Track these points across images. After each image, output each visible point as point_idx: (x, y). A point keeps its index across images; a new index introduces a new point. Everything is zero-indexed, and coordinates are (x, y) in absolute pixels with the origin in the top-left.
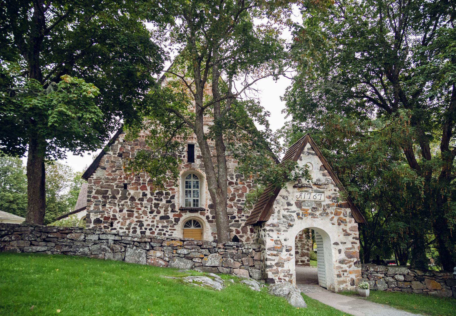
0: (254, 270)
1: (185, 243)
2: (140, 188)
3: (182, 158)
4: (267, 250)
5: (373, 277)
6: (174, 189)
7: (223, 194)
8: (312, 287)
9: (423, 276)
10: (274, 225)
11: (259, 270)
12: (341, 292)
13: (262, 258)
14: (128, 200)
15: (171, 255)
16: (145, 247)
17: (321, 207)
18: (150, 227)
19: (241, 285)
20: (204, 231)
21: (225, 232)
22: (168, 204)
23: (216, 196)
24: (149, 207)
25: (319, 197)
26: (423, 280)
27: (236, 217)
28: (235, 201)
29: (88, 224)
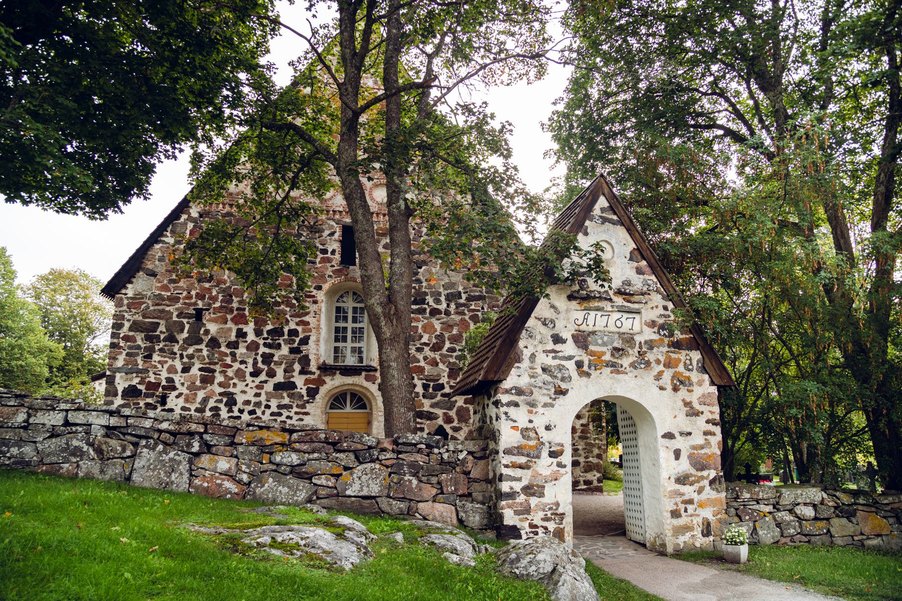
0: (469, 505)
1: (295, 436)
2: (232, 320)
3: (329, 255)
4: (501, 454)
5: (748, 514)
6: (308, 323)
7: (399, 318)
8: (610, 544)
9: (852, 504)
10: (520, 392)
11: (483, 503)
12: (680, 555)
13: (491, 475)
15: (256, 466)
16: (189, 445)
17: (633, 348)
18: (251, 408)
19: (420, 551)
20: (374, 416)
21: (402, 410)
22: (293, 356)
23: (383, 324)
25: (629, 324)
26: (854, 515)
27: (446, 385)
28: (444, 351)
29: (110, 398)
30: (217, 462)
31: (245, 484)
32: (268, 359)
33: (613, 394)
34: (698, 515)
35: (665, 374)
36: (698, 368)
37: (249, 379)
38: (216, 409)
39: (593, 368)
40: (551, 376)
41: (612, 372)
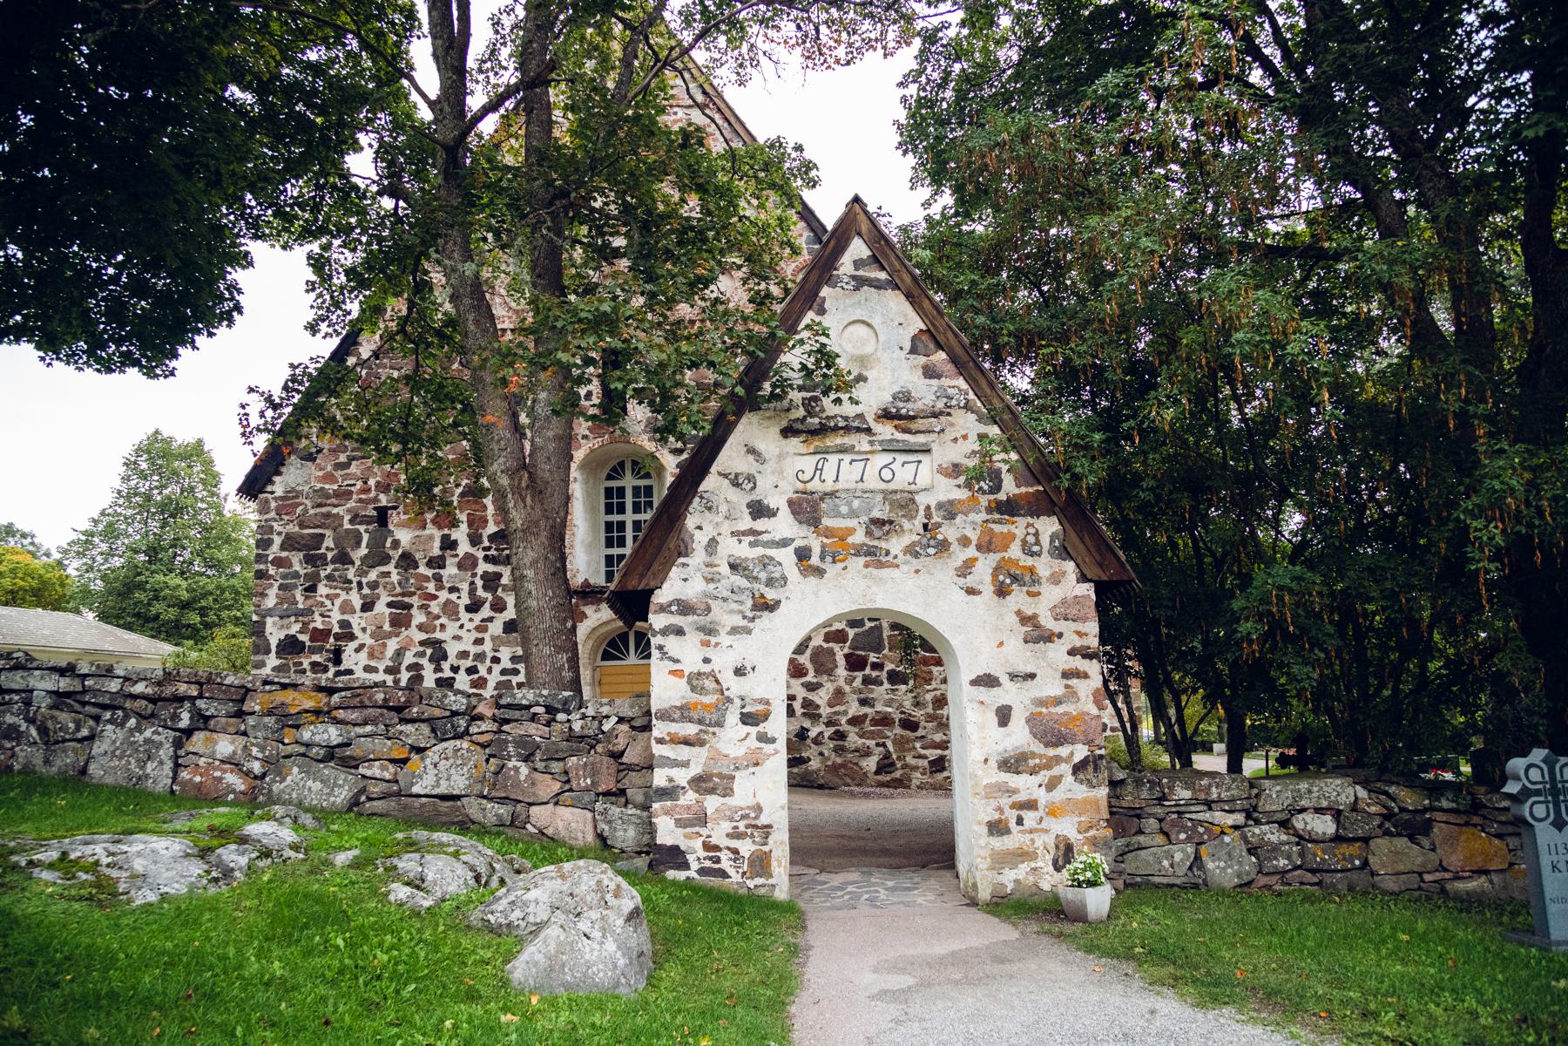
0: (615, 811)
1: (336, 698)
5: (1184, 829)
9: (1425, 810)
10: (685, 608)
14: (390, 567)
16: (175, 717)
17: (911, 518)
18: (469, 663)
24: (465, 587)
25: (904, 473)
26: (1426, 828)
29: (259, 657)
30: (216, 743)
31: (256, 777)
32: (491, 581)
33: (869, 606)
34: (1046, 831)
35: (979, 564)
36: (1052, 547)
37: (464, 616)
38: (415, 667)
39: (829, 559)
40: (747, 578)
41: (866, 566)
